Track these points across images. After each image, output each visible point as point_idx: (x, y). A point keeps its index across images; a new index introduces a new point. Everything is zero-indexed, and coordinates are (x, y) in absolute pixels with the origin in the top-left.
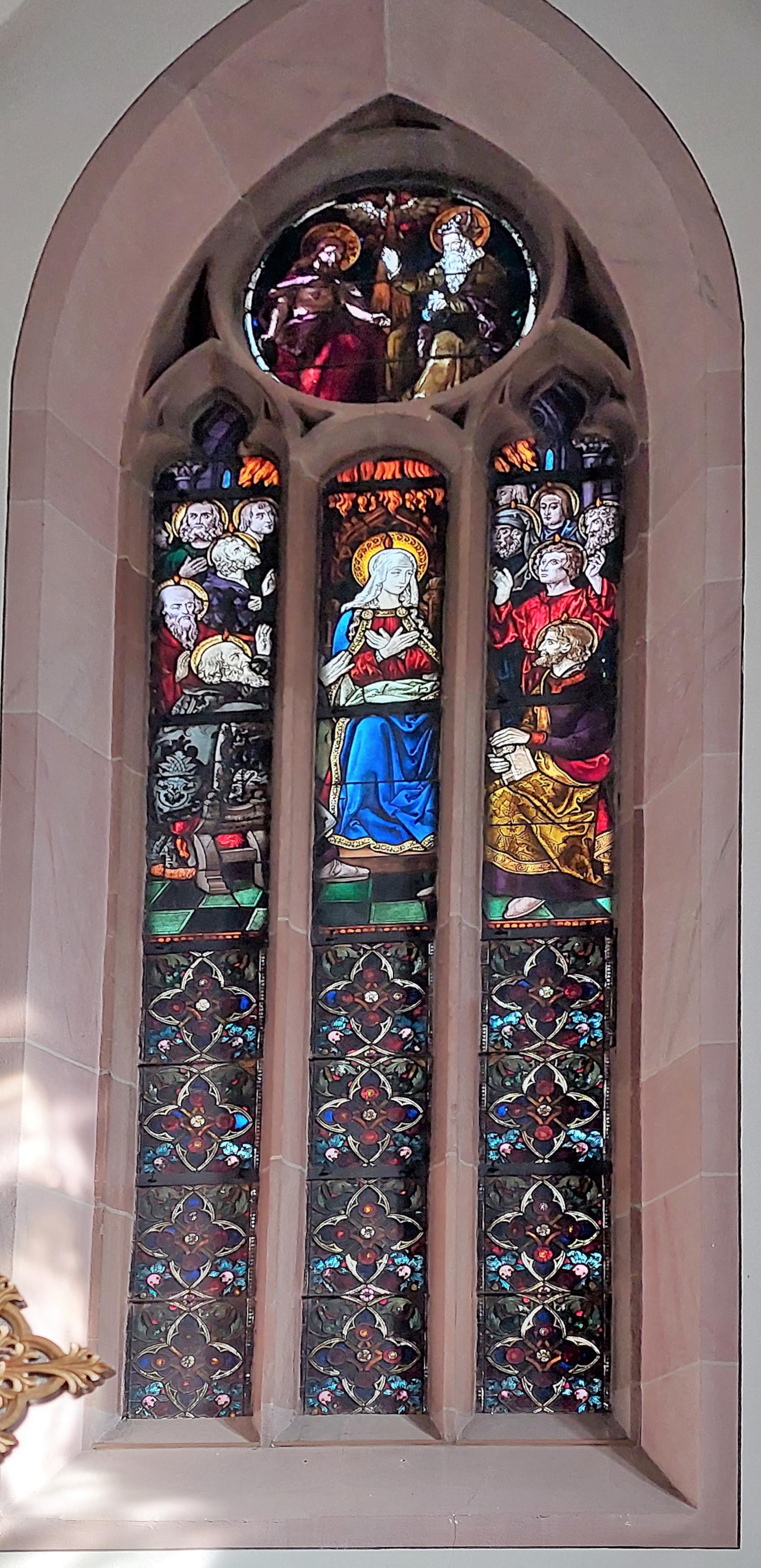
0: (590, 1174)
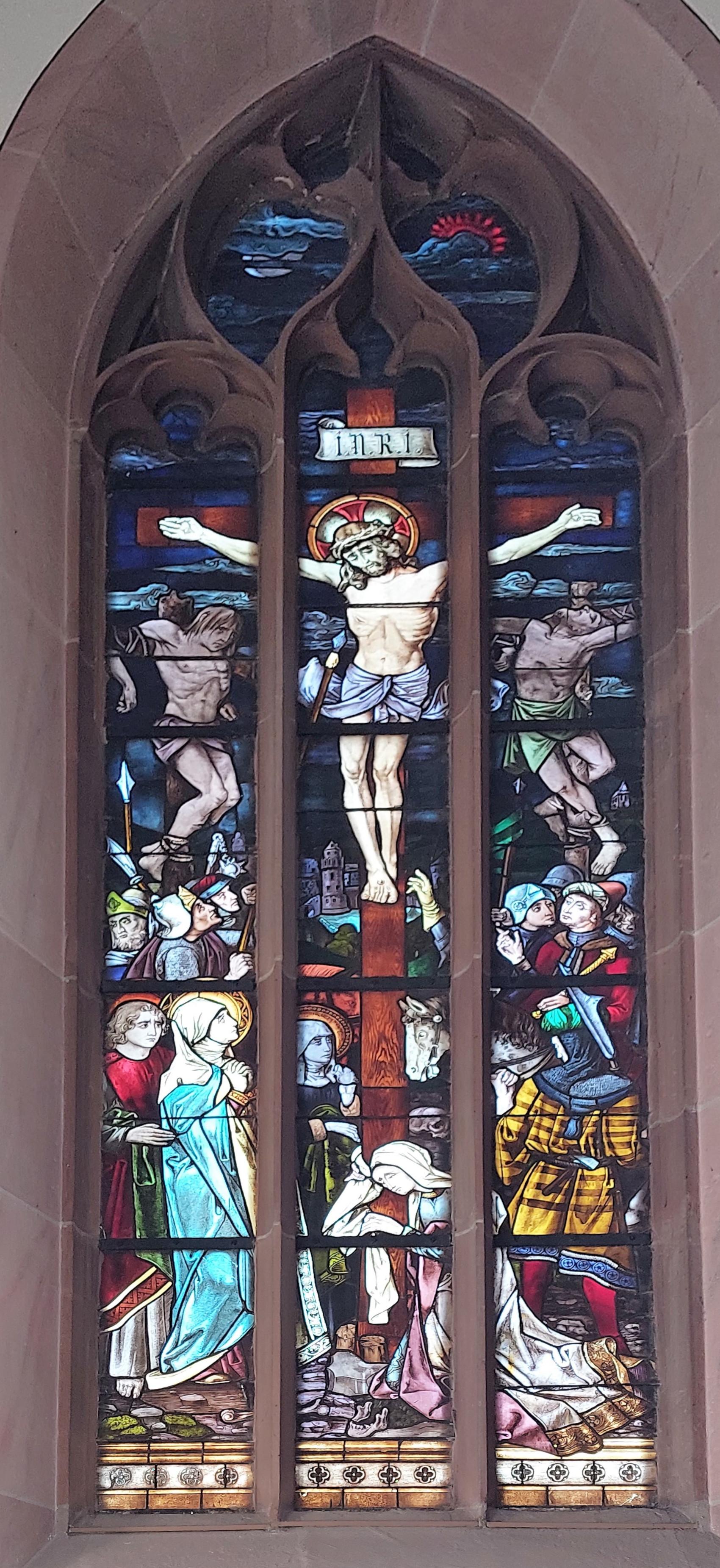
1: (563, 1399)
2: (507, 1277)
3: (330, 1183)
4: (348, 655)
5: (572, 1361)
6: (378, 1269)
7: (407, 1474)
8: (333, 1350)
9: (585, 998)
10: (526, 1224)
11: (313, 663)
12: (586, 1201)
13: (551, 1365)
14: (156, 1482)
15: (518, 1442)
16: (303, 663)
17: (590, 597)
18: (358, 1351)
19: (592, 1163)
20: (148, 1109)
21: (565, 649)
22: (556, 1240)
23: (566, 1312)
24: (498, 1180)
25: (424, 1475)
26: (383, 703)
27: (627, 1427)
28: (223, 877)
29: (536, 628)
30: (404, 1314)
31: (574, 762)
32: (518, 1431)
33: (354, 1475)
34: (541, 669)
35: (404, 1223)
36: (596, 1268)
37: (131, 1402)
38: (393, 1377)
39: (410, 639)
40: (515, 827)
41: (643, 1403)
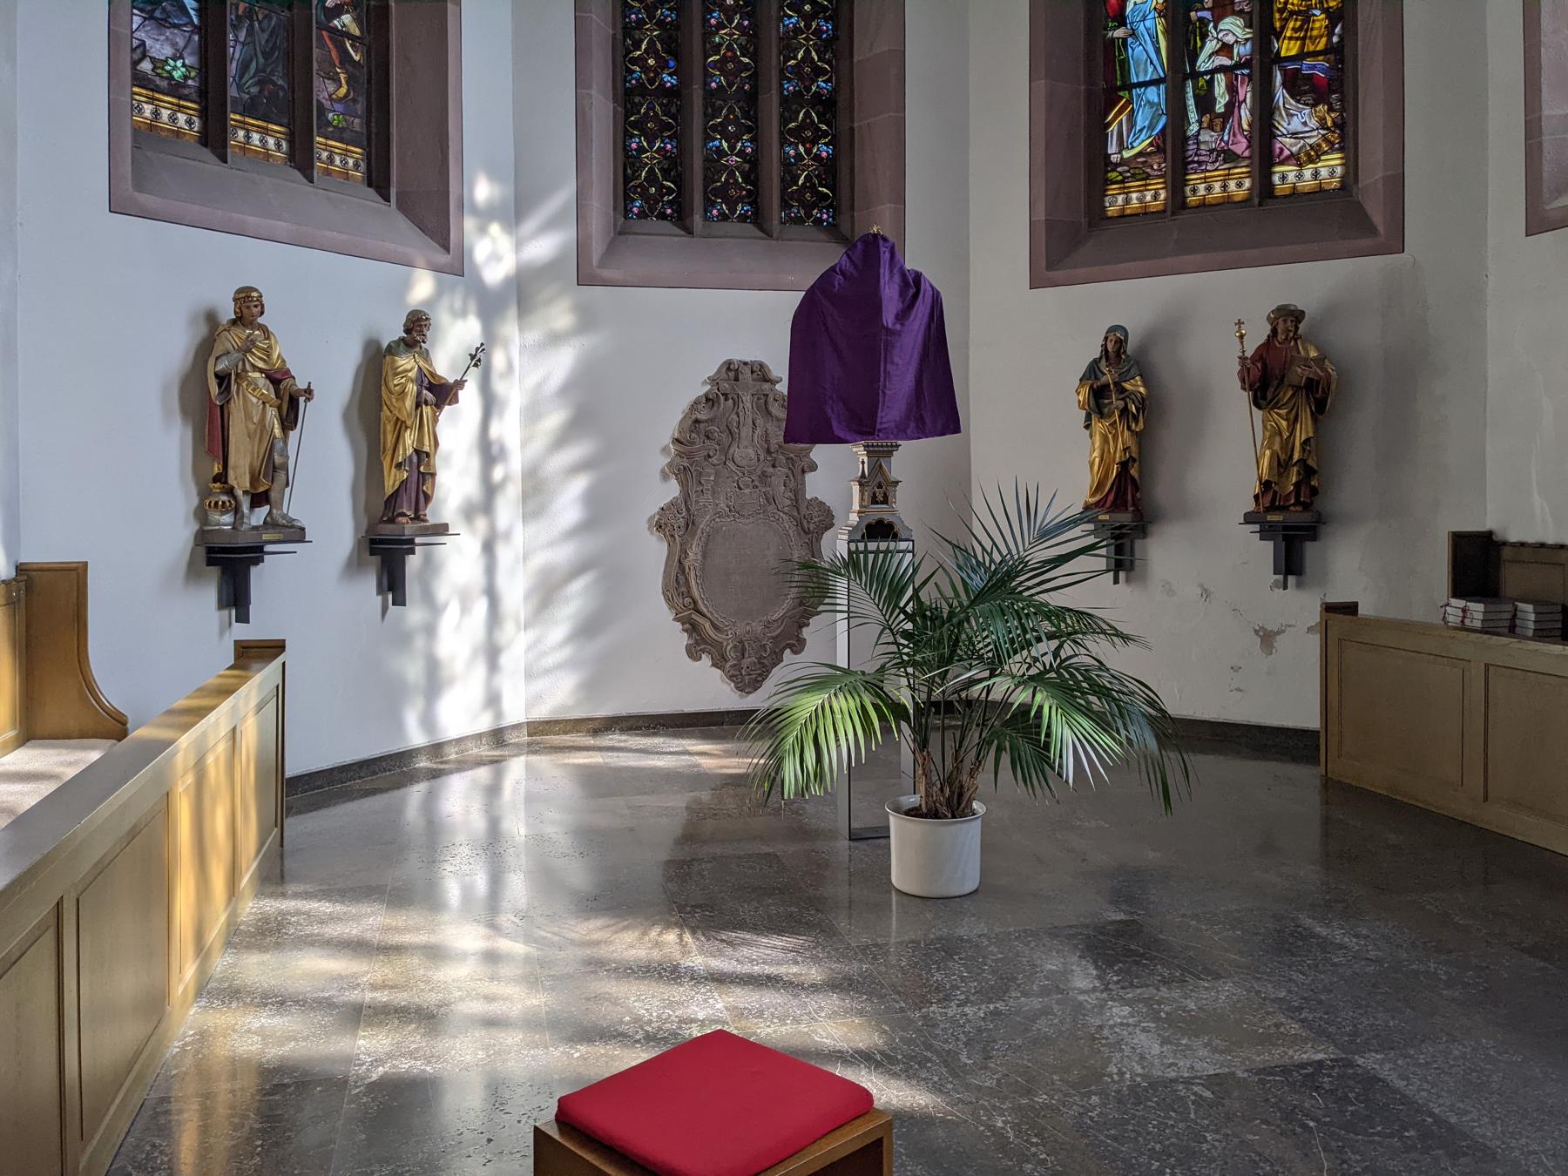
0: (828, 106)
6: (1221, 80)
7: (1232, 185)
13: (1298, 122)
14: (1127, 201)
15: (1282, 163)
18: (1211, 127)
19: (1317, 12)
20: (1121, 21)
23: (1305, 93)
25: (1239, 185)
27: (1332, 150)
30: (1231, 106)
33: (1209, 189)
35: (1231, 58)
36: (1317, 67)
37: (1117, 165)
41: (1344, 135)
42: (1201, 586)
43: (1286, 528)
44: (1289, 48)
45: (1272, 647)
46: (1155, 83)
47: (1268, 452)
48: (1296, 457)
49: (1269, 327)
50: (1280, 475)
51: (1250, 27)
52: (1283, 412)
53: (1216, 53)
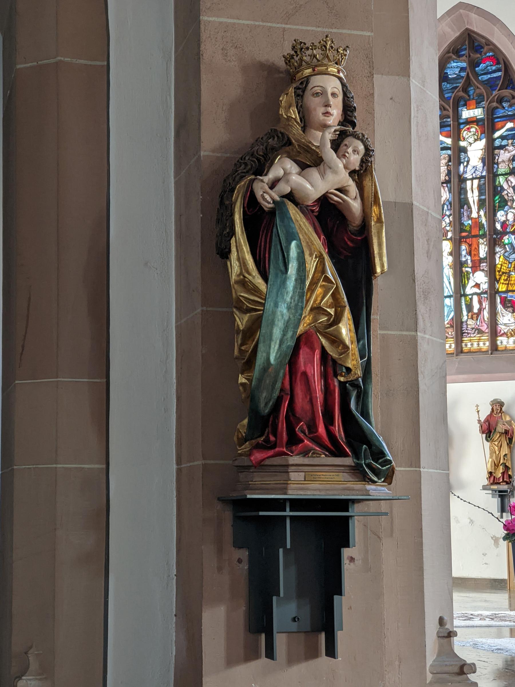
1: (508, 326)
2: (498, 300)
3: (466, 282)
4: (468, 162)
5: (510, 318)
6: (475, 299)
8: (468, 318)
9: (512, 236)
10: (502, 288)
11: (462, 164)
12: (512, 282)
15: (501, 336)
16: (460, 165)
17: (512, 144)
21: (507, 156)
22: (507, 291)
23: (509, 307)
24: (496, 279)
25: (484, 344)
26: (474, 172)
28: (446, 215)
29: (502, 151)
30: (480, 310)
31: (509, 182)
32: (501, 334)
33: (472, 345)
34: (503, 161)
35: (480, 289)
38: (478, 324)
39: (479, 157)
40: (499, 198)
42: (469, 518)
43: (500, 491)
44: (502, 288)
45: (499, 544)
46: (449, 297)
47: (490, 460)
48: (501, 462)
49: (491, 407)
50: (495, 469)
51: (487, 277)
52: (496, 443)
53: (474, 286)
